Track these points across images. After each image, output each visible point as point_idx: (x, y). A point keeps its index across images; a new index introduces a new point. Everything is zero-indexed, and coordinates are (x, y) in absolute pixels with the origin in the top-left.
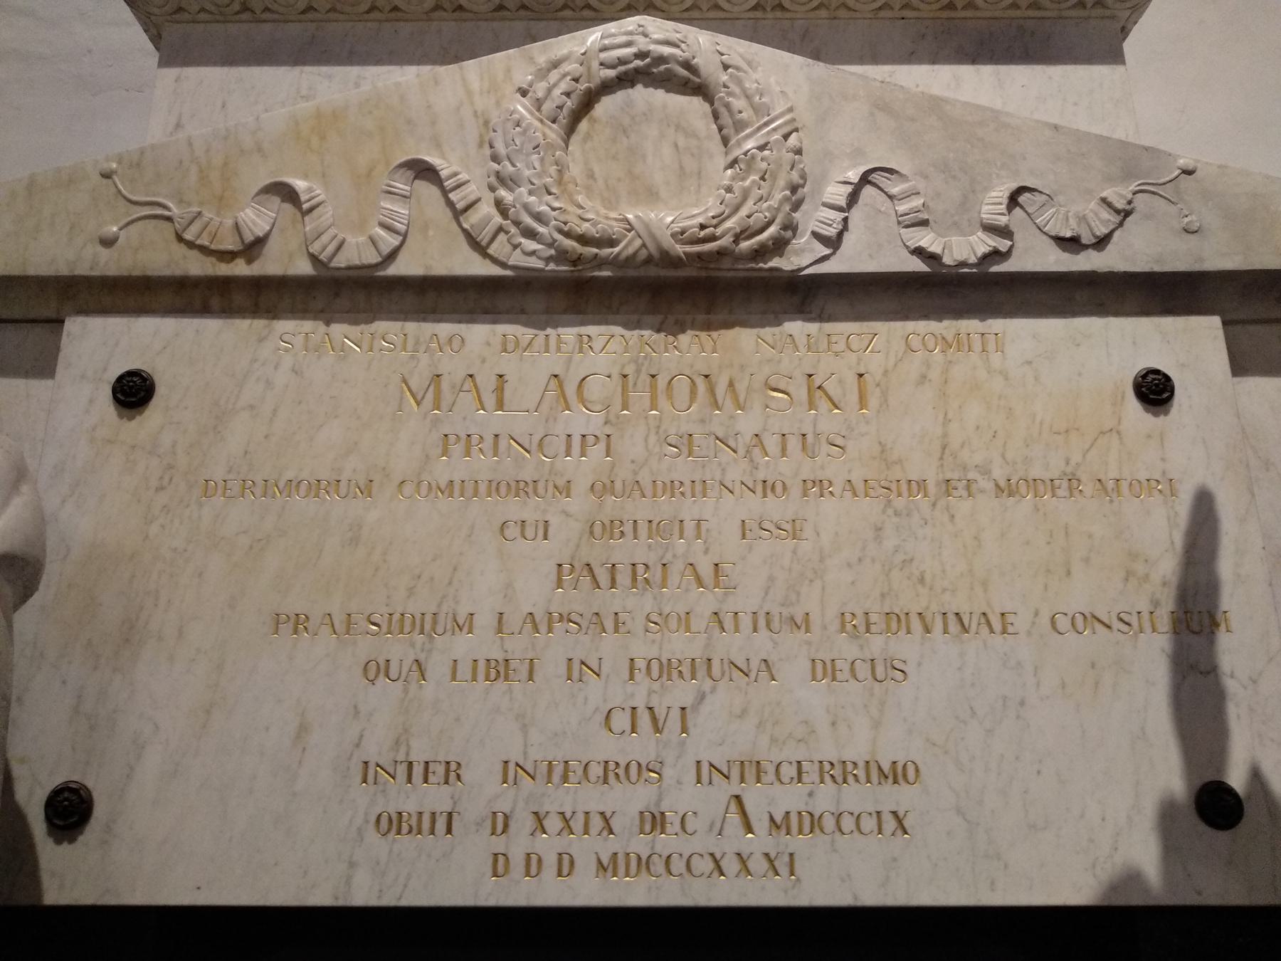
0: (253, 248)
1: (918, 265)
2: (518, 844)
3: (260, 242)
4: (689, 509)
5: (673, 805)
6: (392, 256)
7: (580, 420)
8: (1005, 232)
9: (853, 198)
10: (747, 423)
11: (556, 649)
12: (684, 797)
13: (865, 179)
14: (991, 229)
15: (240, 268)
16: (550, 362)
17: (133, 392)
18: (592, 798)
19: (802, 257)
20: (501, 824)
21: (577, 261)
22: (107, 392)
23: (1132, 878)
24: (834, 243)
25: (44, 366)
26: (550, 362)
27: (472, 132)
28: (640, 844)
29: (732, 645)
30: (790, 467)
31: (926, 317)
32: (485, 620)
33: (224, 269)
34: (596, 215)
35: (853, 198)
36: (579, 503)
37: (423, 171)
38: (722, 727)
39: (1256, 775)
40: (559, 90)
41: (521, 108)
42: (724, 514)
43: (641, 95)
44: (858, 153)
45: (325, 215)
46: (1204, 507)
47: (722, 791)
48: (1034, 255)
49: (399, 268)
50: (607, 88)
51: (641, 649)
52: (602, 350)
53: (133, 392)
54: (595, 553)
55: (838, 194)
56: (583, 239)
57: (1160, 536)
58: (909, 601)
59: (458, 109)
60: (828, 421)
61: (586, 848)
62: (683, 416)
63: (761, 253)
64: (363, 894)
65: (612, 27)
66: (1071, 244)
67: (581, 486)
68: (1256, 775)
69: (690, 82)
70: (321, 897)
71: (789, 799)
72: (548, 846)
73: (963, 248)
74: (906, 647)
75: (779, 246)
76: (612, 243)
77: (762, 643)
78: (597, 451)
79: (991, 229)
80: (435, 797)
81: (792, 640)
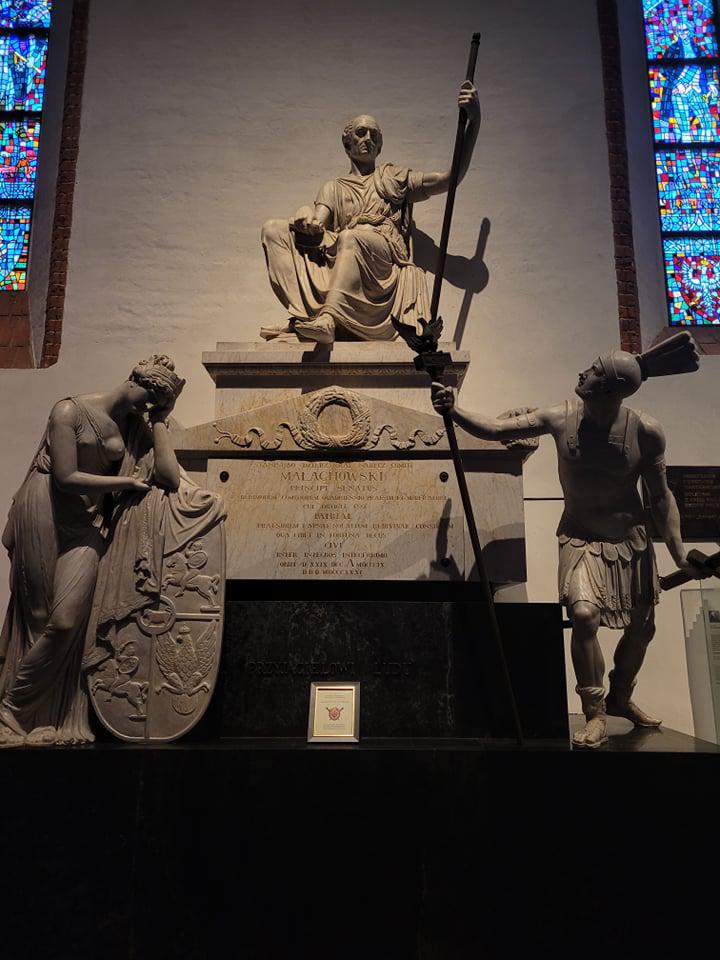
0: (249, 445)
1: (394, 449)
2: (308, 568)
3: (251, 443)
4: (343, 502)
5: (338, 561)
6: (279, 447)
7: (320, 483)
8: (414, 441)
9: (381, 433)
10: (356, 484)
11: (316, 530)
12: (340, 559)
13: (384, 428)
14: (410, 440)
15: (246, 449)
16: (314, 470)
17: (224, 477)
18: (323, 560)
19: (369, 447)
20: (305, 565)
21: (319, 447)
22: (219, 477)
23: (424, 576)
24: (376, 444)
25: (204, 469)
26: (314, 470)
27: (296, 415)
28: (332, 569)
29: (351, 531)
30: (364, 493)
31: (357, 387)
32: (301, 526)
33: (243, 449)
34: (323, 437)
35: (381, 433)
36: (320, 501)
37: (285, 426)
38: (348, 547)
39: (451, 556)
40: (315, 406)
41: (306, 410)
42: (350, 503)
43: (334, 406)
44: (383, 422)
45: (264, 436)
46: (449, 501)
47: (347, 559)
48: (420, 447)
49: (282, 449)
50: (327, 405)
51: (333, 531)
52: (325, 467)
53: (224, 477)
54: (324, 512)
55: (377, 432)
56: (321, 443)
57: (440, 507)
58: (388, 521)
59: (609, 564)
60: (373, 483)
61: (320, 569)
62: (342, 482)
63: (360, 446)
64: (278, 577)
65: (328, 389)
66: (428, 444)
67: (320, 497)
68: (451, 556)
69: (345, 404)
70: (270, 578)
71: (361, 560)
72: (314, 569)
73: (403, 444)
74: (386, 531)
75: (364, 444)
76: (326, 444)
77: (357, 530)
78: (323, 490)
79: (410, 440)
80: (292, 559)
81: (363, 529)
